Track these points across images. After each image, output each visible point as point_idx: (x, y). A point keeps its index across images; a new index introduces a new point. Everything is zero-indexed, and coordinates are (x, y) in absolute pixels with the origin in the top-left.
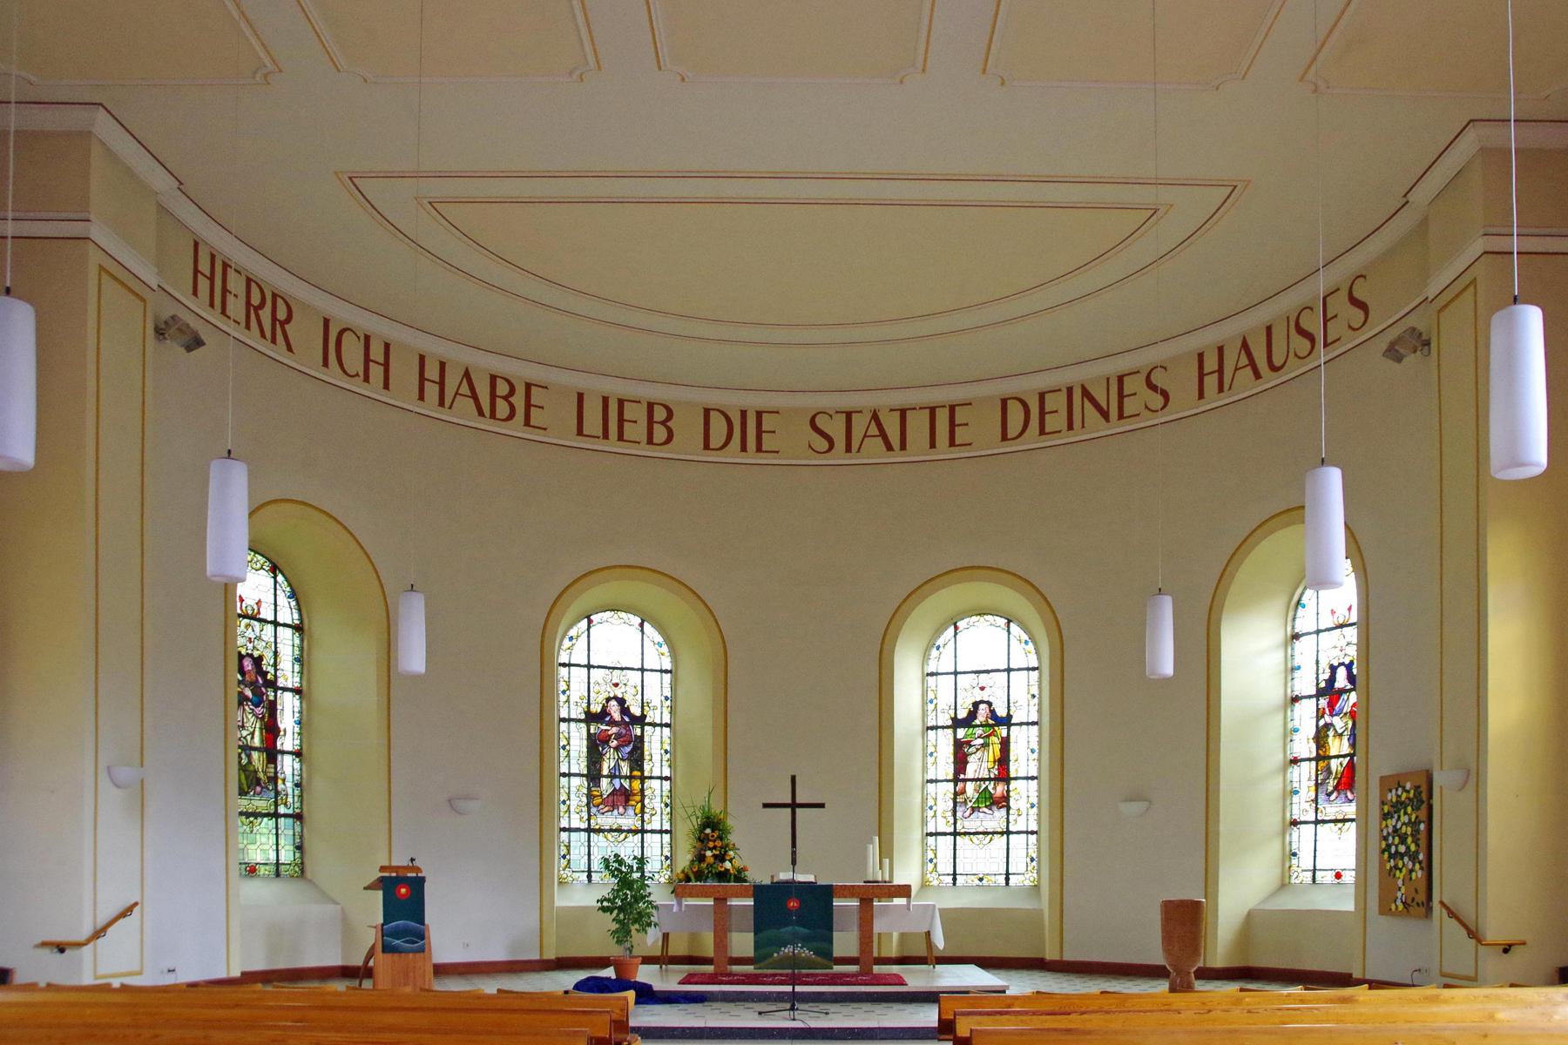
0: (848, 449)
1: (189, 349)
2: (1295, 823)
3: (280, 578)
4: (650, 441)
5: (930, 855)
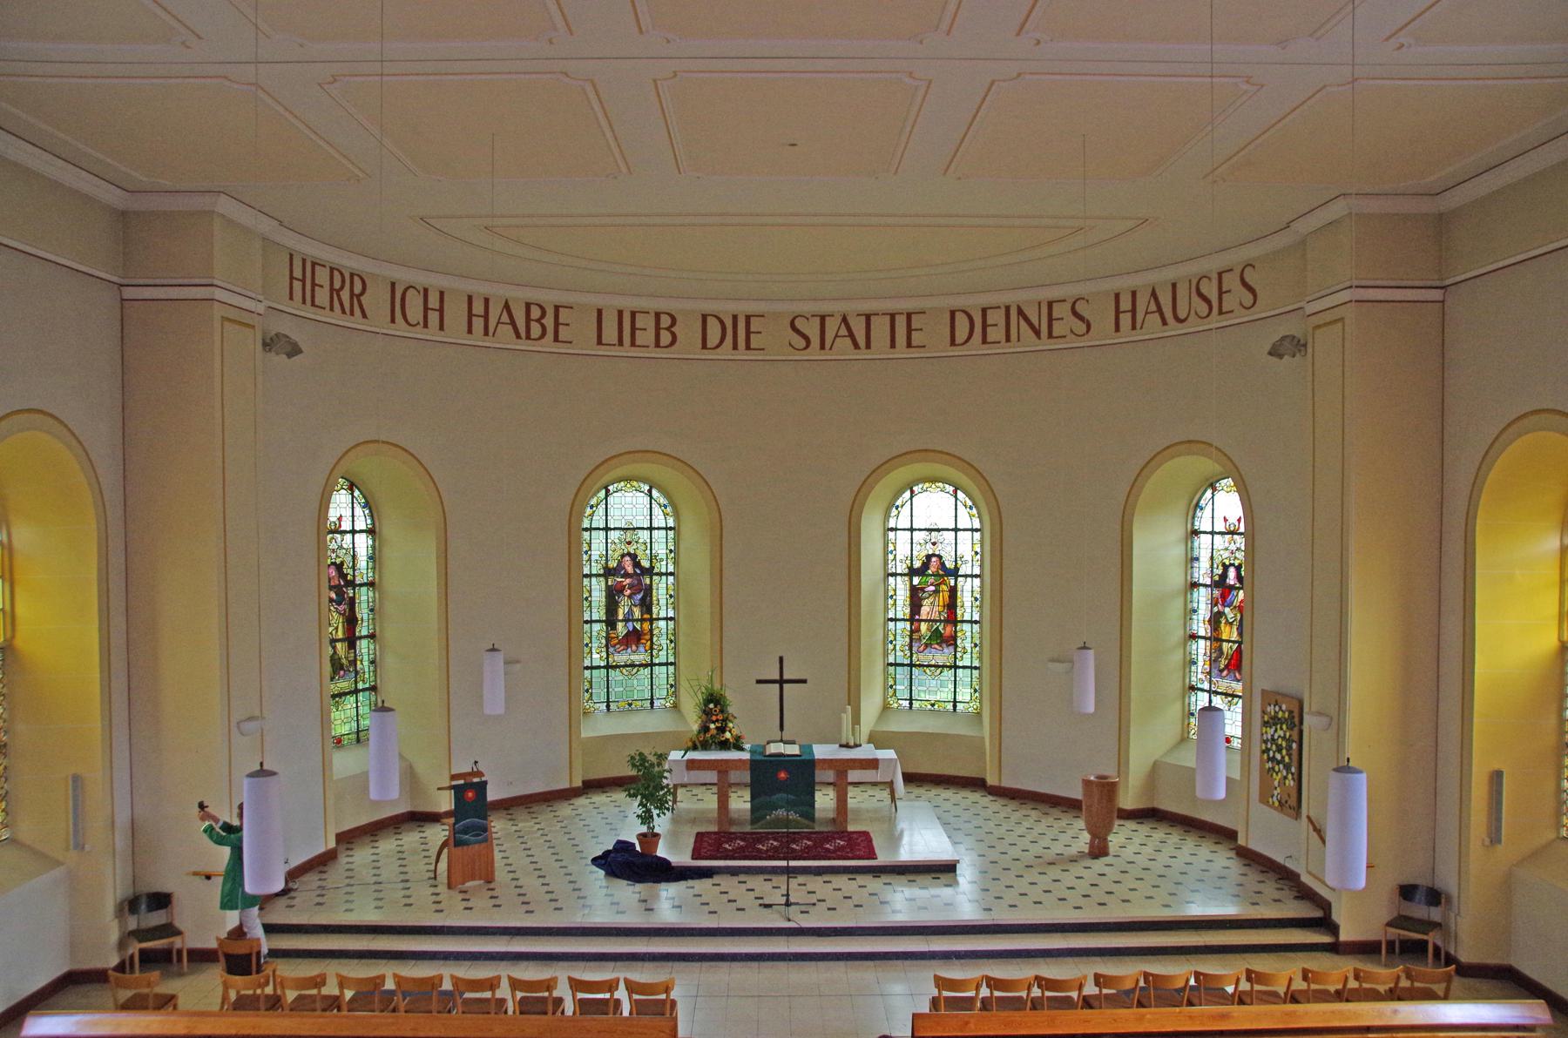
0: (822, 347)
1: (290, 355)
2: (1193, 688)
3: (357, 493)
4: (657, 345)
5: (891, 682)
